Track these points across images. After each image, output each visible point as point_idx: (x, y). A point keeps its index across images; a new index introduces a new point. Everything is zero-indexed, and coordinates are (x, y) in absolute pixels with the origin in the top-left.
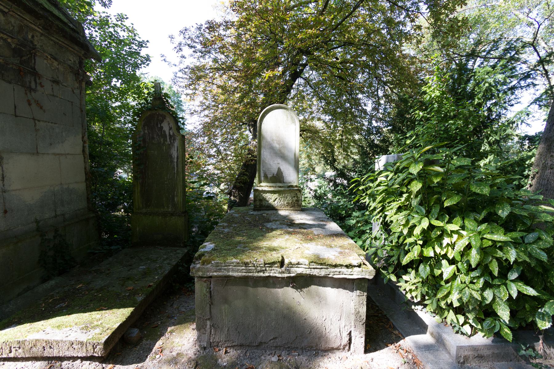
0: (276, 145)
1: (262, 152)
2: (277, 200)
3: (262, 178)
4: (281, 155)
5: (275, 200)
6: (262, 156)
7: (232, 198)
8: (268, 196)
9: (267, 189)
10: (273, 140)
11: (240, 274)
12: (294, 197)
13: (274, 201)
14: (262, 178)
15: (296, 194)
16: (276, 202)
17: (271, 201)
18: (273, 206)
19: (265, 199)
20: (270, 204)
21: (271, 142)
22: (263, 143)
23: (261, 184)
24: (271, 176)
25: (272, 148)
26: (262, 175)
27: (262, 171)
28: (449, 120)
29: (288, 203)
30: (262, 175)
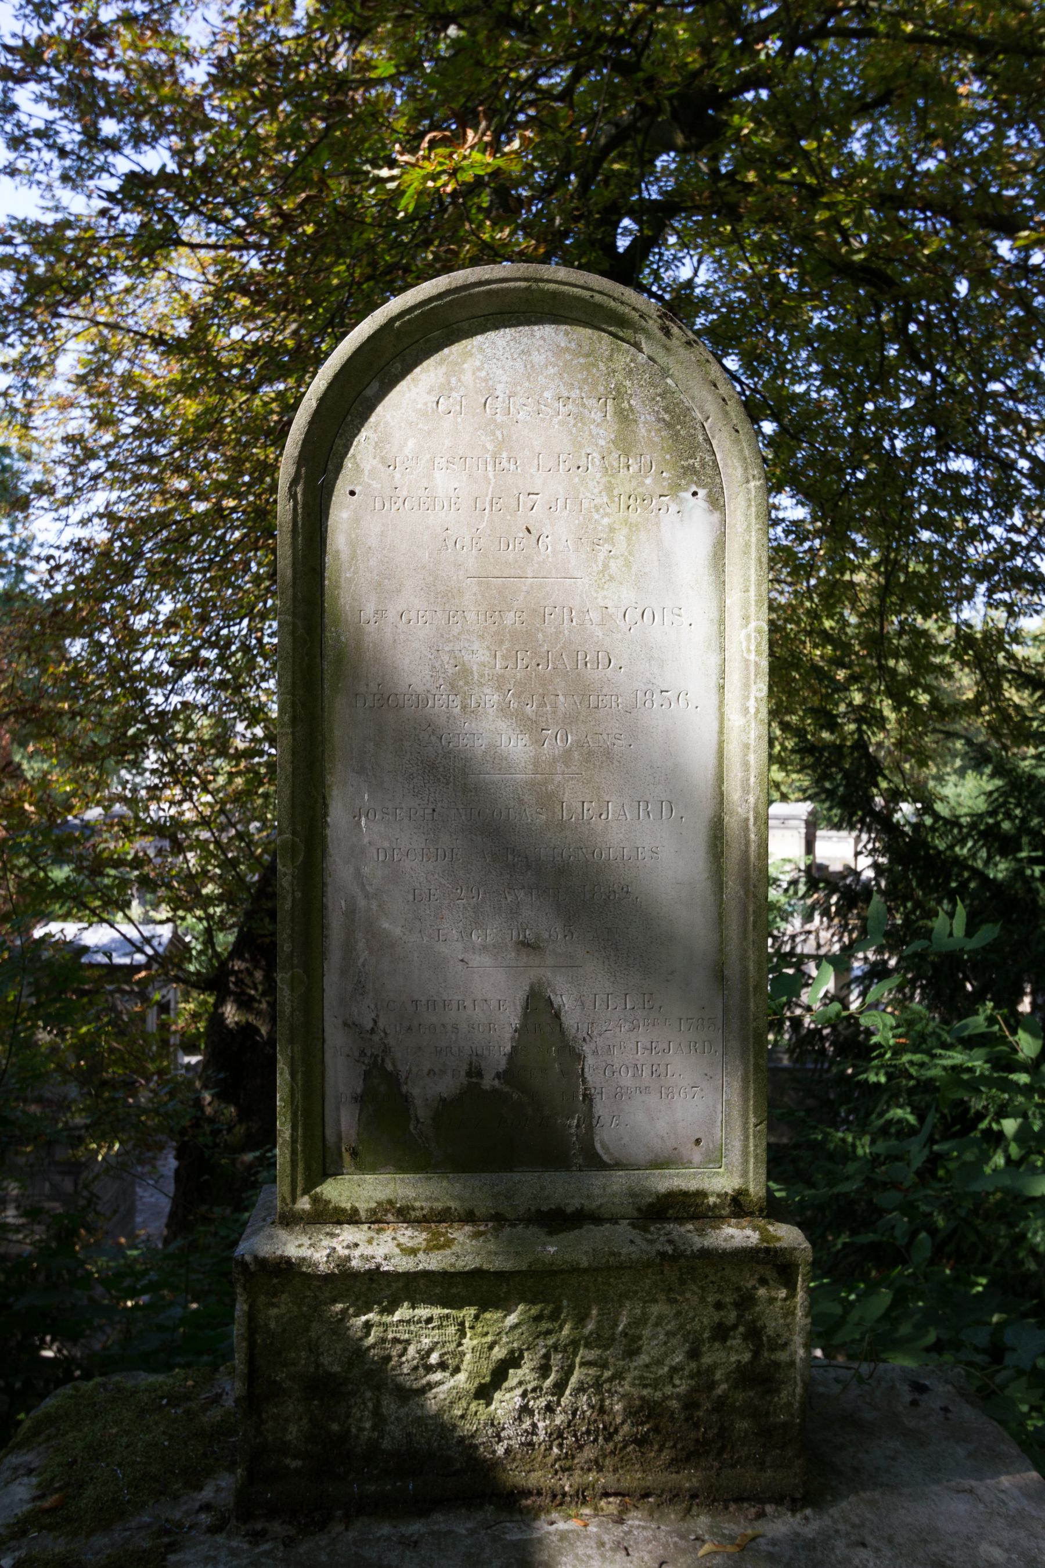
0: (502, 739)
1: (338, 814)
2: (523, 1374)
3: (345, 1121)
4: (547, 877)
5: (499, 1374)
6: (340, 869)
7: (231, 1013)
8: (415, 1331)
9: (383, 1249)
10: (460, 679)
11: (613, 304)
12: (721, 1333)
13: (484, 1393)
14: (345, 1121)
15: (746, 1301)
16: (505, 1403)
17: (448, 1388)
18: (467, 1446)
19: (373, 1376)
20: (441, 1428)
21: (444, 704)
22: (344, 726)
23: (337, 1191)
24: (446, 1086)
25: (441, 773)
26: (341, 1076)
27: (336, 1038)
28: (206, 513)
29: (642, 1411)
30: (341, 1076)
